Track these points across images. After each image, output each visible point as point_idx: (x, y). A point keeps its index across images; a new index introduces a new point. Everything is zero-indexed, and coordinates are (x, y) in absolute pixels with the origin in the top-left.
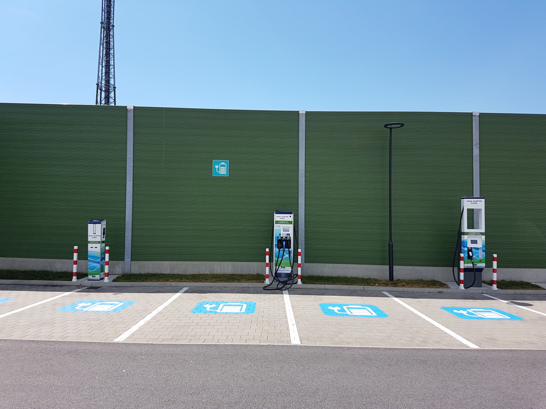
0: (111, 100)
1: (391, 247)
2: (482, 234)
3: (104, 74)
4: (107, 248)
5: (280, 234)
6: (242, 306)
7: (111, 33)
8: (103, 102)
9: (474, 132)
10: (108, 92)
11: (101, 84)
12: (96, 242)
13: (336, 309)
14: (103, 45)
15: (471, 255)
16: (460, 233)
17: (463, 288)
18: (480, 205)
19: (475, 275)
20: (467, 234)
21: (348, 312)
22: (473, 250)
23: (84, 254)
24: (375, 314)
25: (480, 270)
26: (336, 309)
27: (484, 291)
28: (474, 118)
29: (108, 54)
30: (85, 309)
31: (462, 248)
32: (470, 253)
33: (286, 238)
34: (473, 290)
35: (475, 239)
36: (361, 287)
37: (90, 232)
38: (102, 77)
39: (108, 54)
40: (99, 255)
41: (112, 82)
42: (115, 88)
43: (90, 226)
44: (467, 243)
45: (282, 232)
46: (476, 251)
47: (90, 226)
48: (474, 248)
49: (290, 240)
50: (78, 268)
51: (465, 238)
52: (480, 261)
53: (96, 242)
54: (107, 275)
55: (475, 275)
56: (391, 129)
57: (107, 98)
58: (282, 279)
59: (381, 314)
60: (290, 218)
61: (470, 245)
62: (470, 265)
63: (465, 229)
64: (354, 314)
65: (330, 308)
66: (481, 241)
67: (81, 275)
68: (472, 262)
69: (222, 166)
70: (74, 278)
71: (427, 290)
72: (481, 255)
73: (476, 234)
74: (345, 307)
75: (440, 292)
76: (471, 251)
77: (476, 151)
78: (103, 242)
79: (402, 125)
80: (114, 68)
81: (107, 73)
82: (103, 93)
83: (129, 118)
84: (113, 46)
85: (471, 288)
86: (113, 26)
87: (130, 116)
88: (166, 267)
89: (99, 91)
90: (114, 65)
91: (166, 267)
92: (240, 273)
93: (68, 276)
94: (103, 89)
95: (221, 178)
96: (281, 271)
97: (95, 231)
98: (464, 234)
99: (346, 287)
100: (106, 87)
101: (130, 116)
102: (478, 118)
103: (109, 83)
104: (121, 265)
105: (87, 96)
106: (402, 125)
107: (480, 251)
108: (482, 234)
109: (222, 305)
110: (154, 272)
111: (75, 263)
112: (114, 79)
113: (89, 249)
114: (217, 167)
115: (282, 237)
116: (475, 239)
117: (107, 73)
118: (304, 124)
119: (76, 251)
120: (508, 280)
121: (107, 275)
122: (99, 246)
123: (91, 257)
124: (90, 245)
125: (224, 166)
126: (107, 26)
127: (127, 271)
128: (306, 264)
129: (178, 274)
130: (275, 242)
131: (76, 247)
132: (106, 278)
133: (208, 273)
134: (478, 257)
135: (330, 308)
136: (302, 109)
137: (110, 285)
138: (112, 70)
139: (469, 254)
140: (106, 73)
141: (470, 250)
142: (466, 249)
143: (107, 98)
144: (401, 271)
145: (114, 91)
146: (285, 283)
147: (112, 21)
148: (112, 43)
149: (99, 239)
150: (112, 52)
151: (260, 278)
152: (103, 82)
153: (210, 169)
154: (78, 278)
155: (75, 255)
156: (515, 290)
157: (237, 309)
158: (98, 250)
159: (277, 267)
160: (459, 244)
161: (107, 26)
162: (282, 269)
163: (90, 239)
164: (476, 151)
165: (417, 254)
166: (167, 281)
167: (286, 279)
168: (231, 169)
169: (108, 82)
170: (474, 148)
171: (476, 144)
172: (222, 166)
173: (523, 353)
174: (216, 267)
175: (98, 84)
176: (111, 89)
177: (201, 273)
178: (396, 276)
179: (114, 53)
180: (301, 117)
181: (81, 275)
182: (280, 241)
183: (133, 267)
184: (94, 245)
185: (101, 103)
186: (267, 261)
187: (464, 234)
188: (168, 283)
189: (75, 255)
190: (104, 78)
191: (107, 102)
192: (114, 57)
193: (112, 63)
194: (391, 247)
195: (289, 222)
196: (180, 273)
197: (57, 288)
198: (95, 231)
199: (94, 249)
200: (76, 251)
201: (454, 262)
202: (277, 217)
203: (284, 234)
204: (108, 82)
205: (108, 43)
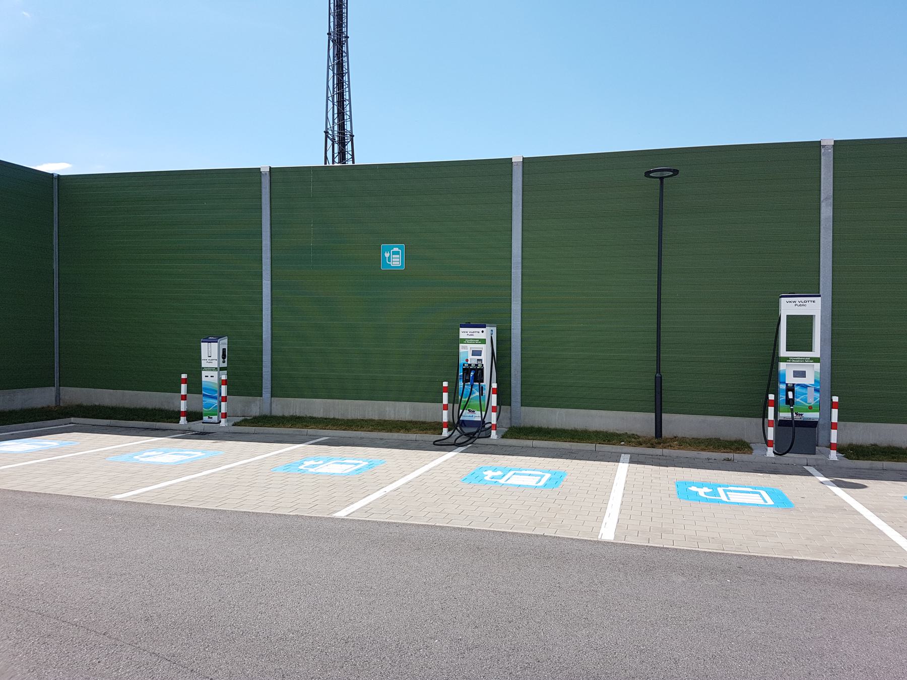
0: (348, 156)
1: (659, 382)
2: (816, 360)
3: (336, 116)
4: (224, 377)
5: (467, 360)
6: (542, 476)
7: (344, 49)
8: (337, 160)
9: (822, 177)
10: (342, 143)
11: (333, 131)
12: (211, 369)
13: (702, 492)
14: (333, 70)
16: (775, 359)
17: (773, 455)
19: (794, 433)
20: (786, 359)
21: (724, 498)
22: (796, 388)
23: (196, 386)
24: (770, 502)
25: (813, 424)
26: (702, 492)
27: (810, 462)
28: (823, 150)
29: (340, 84)
30: (311, 470)
33: (477, 365)
34: (790, 457)
35: (803, 373)
36: (589, 447)
37: (204, 355)
38: (333, 120)
39: (340, 84)
40: (216, 387)
41: (348, 127)
42: (352, 136)
43: (204, 346)
44: (784, 375)
45: (470, 357)
46: (803, 391)
47: (204, 346)
48: (798, 385)
49: (482, 370)
50: (228, 407)
52: (810, 408)
53: (211, 369)
54: (225, 416)
55: (794, 433)
56: (662, 179)
57: (342, 153)
58: (467, 430)
59: (781, 501)
60: (486, 333)
61: (790, 380)
63: (783, 352)
64: (732, 500)
65: (694, 489)
66: (813, 372)
67: (194, 416)
68: (792, 410)
69: (395, 253)
70: (183, 420)
71: (705, 454)
72: (812, 398)
73: (804, 360)
74: (720, 490)
75: (728, 460)
77: (826, 212)
78: (222, 369)
79: (676, 172)
80: (350, 104)
81: (341, 114)
82: (336, 146)
83: (263, 186)
84: (348, 69)
85: (787, 455)
86: (347, 37)
87: (266, 182)
88: (317, 407)
89: (329, 142)
90: (350, 100)
91: (317, 407)
92: (422, 419)
93: (174, 416)
94: (337, 139)
95: (394, 274)
96: (466, 416)
97: (211, 353)
99: (567, 445)
100: (341, 138)
101: (266, 182)
102: (831, 151)
103: (344, 129)
104: (258, 403)
105: (310, 152)
106: (676, 172)
107: (811, 390)
109: (511, 473)
110: (302, 415)
111: (184, 398)
112: (351, 121)
113: (204, 379)
114: (387, 255)
115: (470, 365)
116: (803, 373)
117: (341, 114)
118: (520, 179)
119: (185, 381)
120: (885, 444)
121: (225, 416)
122: (215, 374)
123: (206, 389)
124: (204, 373)
125: (398, 253)
126: (338, 39)
127: (266, 412)
128: (523, 408)
129: (334, 419)
130: (461, 370)
131: (184, 376)
132: (223, 420)
133: (376, 418)
135: (694, 489)
136: (264, 165)
137: (227, 430)
138: (348, 108)
139: (787, 395)
140: (338, 113)
141: (791, 388)
142: (782, 387)
143: (342, 153)
144: (677, 423)
145: (352, 140)
146: (471, 437)
147: (344, 30)
148: (345, 64)
149: (215, 364)
150: (346, 78)
151: (437, 427)
152: (336, 128)
153: (378, 259)
154: (188, 421)
155: (184, 387)
156: (866, 460)
157: (531, 481)
158: (215, 380)
159: (484, 413)
161: (338, 39)
162: (471, 414)
163: (204, 364)
164: (826, 212)
165: (692, 393)
166: (306, 427)
167: (474, 430)
168: (408, 258)
169: (342, 127)
170: (823, 205)
171: (826, 199)
172: (395, 253)
173: (300, 520)
174: (387, 409)
175: (326, 132)
176: (348, 138)
177: (367, 417)
178: (665, 433)
179: (349, 81)
180: (514, 168)
181: (194, 416)
182: (467, 371)
183: (274, 405)
184: (209, 373)
185: (333, 162)
186: (445, 401)
188: (305, 430)
189: (184, 387)
190: (336, 121)
191: (343, 159)
192: (349, 87)
193: (346, 97)
194: (659, 382)
195: (480, 340)
196: (337, 417)
197: (159, 432)
198: (211, 353)
199: (209, 379)
200: (185, 381)
202: (464, 333)
203: (473, 360)
204: (342, 127)
205: (340, 65)
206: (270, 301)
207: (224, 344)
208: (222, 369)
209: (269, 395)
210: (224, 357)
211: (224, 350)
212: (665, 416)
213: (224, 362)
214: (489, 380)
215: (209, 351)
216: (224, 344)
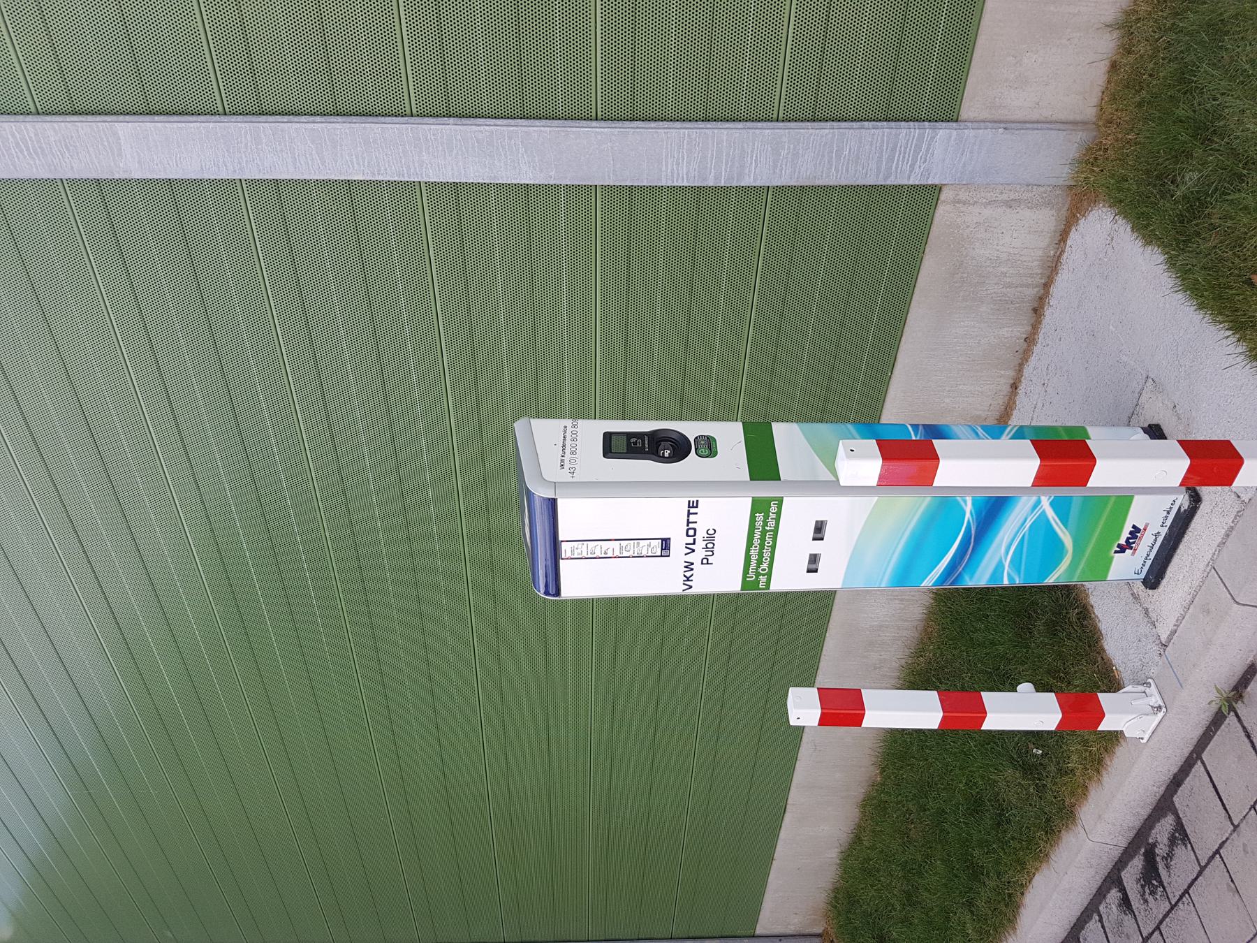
12: (765, 517)
43: (578, 581)
47: (578, 581)
53: (765, 517)
78: (763, 463)
97: (629, 533)
122: (797, 514)
124: (788, 576)
163: (722, 576)
183: (1019, 103)
206: (266, 127)
207: (567, 446)
208: (763, 463)
209: (943, 134)
210: (678, 448)
211: (613, 446)
212: (758, 932)
213: (708, 447)
214: (1147, 547)
215: (627, 548)
216: (567, 446)
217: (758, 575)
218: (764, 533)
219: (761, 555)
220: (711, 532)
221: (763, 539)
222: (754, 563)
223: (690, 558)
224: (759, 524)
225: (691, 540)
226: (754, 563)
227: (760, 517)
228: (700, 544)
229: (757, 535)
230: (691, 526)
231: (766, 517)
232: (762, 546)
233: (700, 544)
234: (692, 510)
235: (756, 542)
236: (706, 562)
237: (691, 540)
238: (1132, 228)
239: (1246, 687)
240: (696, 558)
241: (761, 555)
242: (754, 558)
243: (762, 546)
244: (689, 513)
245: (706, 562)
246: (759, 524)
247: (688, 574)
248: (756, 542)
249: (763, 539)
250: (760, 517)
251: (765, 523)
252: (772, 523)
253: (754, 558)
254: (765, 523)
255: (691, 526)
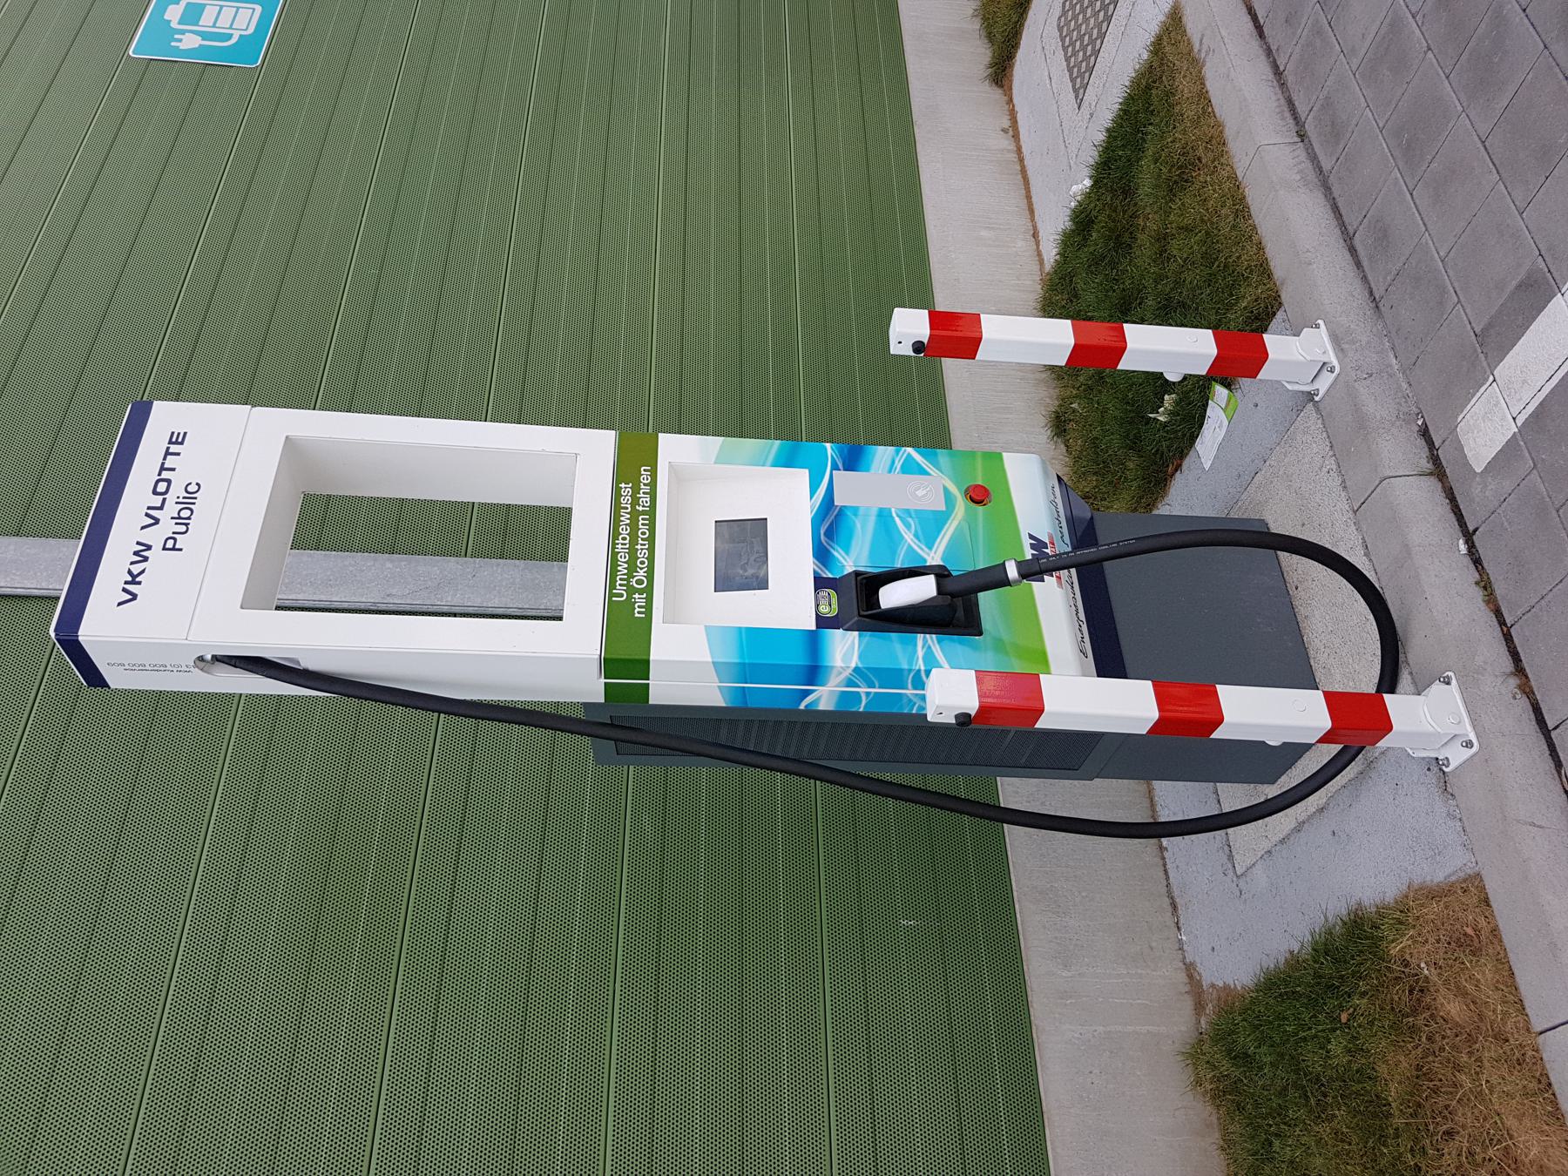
2: (634, 463)
15: (921, 590)
16: (627, 723)
18: (222, 461)
22: (849, 561)
31: (824, 697)
32: (893, 596)
44: (754, 637)
48: (822, 554)
51: (688, 664)
61: (789, 599)
62: (1055, 604)
63: (555, 655)
66: (713, 478)
73: (633, 521)
76: (868, 584)
98: (626, 660)
101: (936, 332)
107: (850, 488)
108: (634, 463)
116: (715, 558)
134: (931, 524)
139: (910, 620)
141: (858, 600)
160: (758, 738)
187: (626, 660)
201: (953, 788)
217: (631, 591)
218: (635, 515)
219: (632, 553)
220: (192, 488)
221: (634, 525)
222: (623, 569)
223: (146, 536)
224: (626, 501)
225: (157, 501)
226: (623, 569)
227: (626, 489)
228: (171, 509)
229: (625, 518)
230: (165, 475)
231: (636, 490)
232: (633, 536)
233: (171, 509)
234: (173, 448)
235: (624, 532)
236: (171, 546)
237: (157, 501)
238: (1108, 130)
239: (1270, 276)
240: (155, 536)
241: (632, 553)
242: (623, 559)
243: (633, 536)
244: (167, 453)
245: (171, 546)
246: (626, 501)
247: (136, 569)
248: (624, 532)
249: (634, 525)
250: (626, 489)
251: (635, 501)
252: (645, 500)
253: (623, 559)
254: (635, 501)
255: (165, 475)
